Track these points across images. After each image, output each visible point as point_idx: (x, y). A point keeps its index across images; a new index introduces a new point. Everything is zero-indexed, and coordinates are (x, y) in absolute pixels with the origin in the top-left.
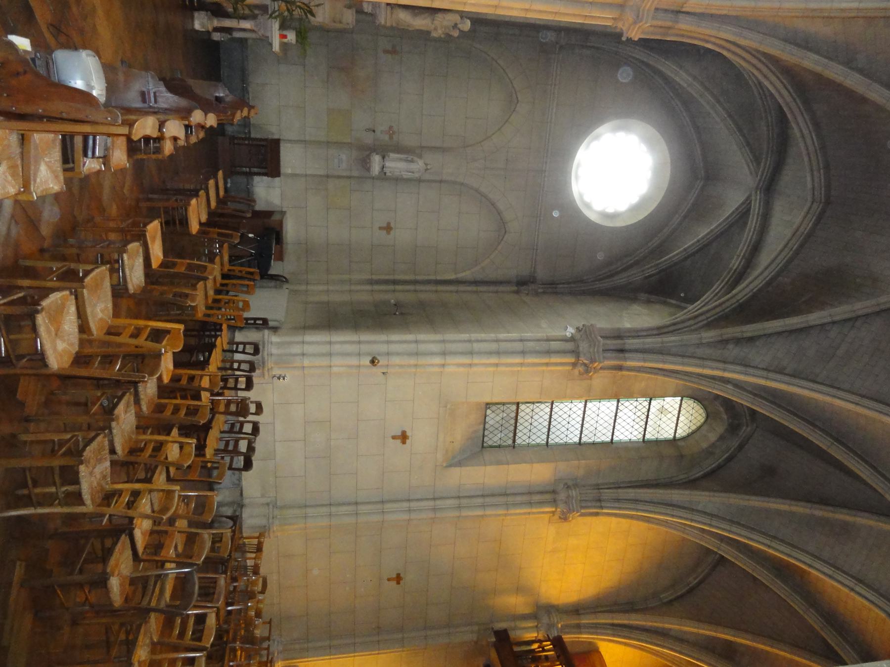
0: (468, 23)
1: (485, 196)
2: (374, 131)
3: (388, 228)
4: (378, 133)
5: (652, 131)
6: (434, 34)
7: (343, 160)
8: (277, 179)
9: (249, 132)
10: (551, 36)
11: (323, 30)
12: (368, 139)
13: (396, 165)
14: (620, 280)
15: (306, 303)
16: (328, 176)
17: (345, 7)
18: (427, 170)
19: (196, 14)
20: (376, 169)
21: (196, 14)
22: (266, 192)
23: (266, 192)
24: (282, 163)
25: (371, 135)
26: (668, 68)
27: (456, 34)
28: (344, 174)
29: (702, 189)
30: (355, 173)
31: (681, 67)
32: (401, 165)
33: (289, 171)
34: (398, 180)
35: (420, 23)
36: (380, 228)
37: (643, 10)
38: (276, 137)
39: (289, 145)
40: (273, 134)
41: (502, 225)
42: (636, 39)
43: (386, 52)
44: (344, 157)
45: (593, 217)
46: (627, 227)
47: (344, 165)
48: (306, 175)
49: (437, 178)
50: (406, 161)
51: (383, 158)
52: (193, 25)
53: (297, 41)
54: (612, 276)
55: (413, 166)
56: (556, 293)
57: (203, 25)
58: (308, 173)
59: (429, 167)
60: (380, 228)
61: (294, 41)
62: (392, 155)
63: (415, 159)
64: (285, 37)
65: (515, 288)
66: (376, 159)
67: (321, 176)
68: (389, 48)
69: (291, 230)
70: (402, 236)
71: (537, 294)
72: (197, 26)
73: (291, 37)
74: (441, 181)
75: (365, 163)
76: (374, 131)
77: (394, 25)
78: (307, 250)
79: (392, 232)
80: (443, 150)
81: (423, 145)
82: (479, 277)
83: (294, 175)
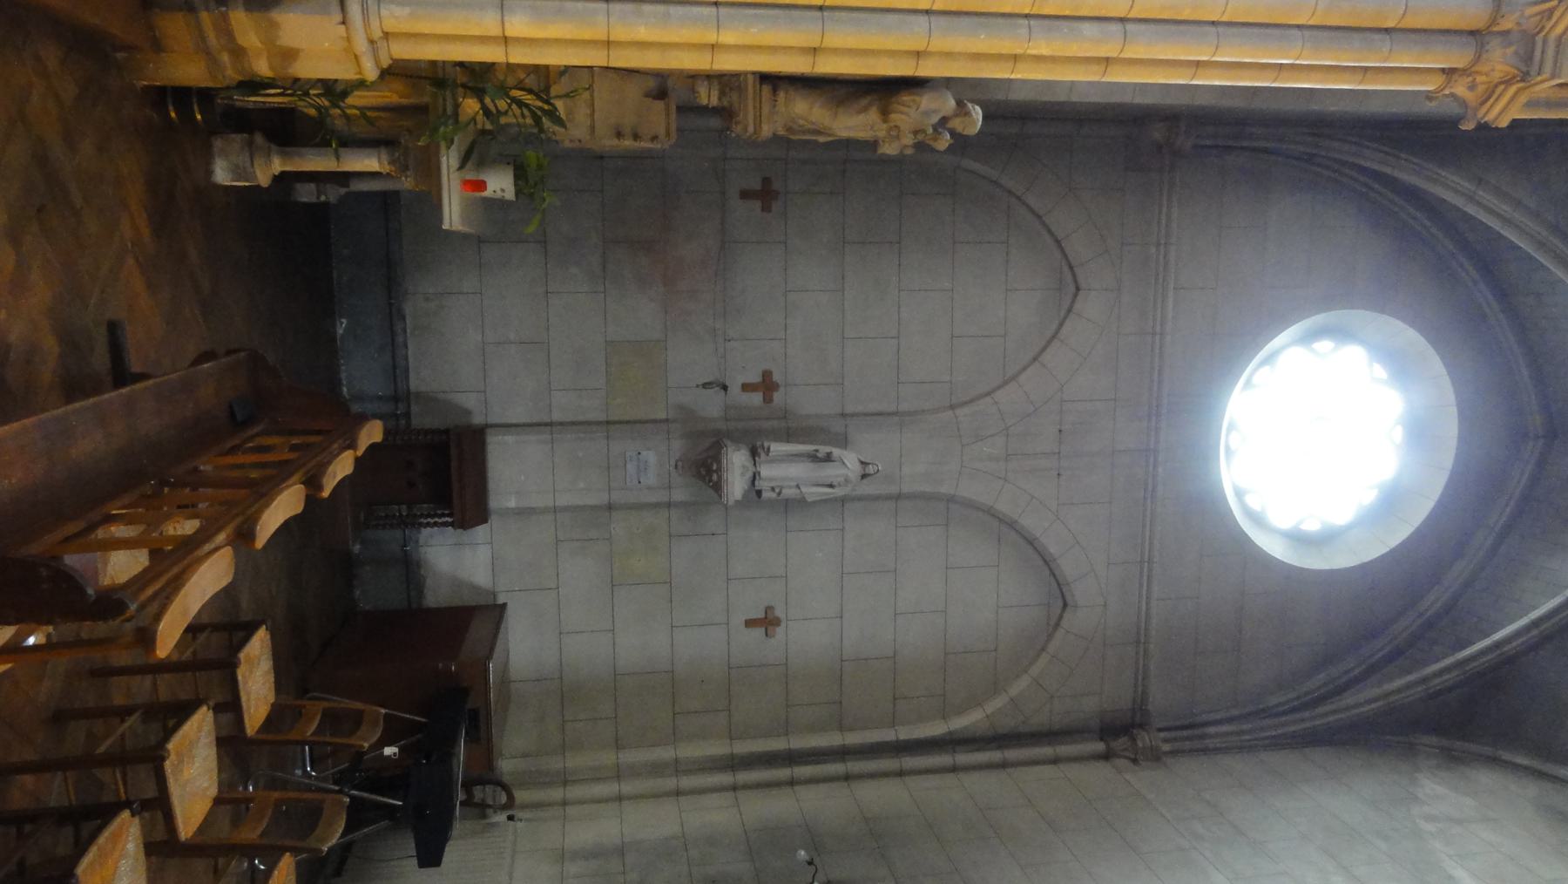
0: (977, 113)
1: (1012, 524)
2: (725, 388)
3: (767, 622)
4: (735, 389)
5: (1408, 336)
6: (889, 149)
7: (652, 465)
8: (481, 531)
9: (407, 415)
10: (1158, 133)
11: (591, 160)
12: (711, 406)
13: (785, 470)
14: (1365, 699)
15: (562, 856)
16: (610, 507)
17: (647, 95)
18: (864, 476)
19: (218, 143)
20: (736, 485)
21: (218, 143)
22: (455, 560)
23: (455, 560)
24: (491, 485)
25: (715, 395)
26: (1451, 187)
27: (944, 142)
28: (653, 499)
29: (1541, 464)
30: (679, 495)
31: (1480, 181)
32: (798, 471)
33: (512, 503)
34: (790, 506)
35: (854, 124)
36: (750, 623)
37: (1545, 41)
38: (478, 420)
39: (510, 439)
40: (468, 413)
41: (1061, 598)
42: (1504, 123)
43: (745, 195)
44: (651, 457)
45: (1275, 548)
46: (1363, 567)
47: (651, 479)
48: (555, 510)
49: (894, 489)
50: (813, 458)
51: (754, 453)
52: (209, 173)
53: (518, 193)
54: (1340, 691)
55: (830, 472)
56: (1205, 751)
57: (238, 172)
58: (563, 501)
59: (871, 469)
60: (750, 623)
61: (510, 195)
62: (777, 448)
63: (836, 452)
64: (481, 186)
65: (1100, 747)
66: (736, 461)
67: (593, 508)
68: (756, 185)
69: (523, 647)
70: (808, 636)
71: (1156, 757)
72: (222, 174)
73: (500, 184)
74: (898, 497)
75: (704, 468)
76: (725, 388)
77: (781, 132)
78: (566, 693)
79: (780, 630)
80: (898, 418)
81: (849, 409)
82: (1007, 724)
83: (523, 513)
